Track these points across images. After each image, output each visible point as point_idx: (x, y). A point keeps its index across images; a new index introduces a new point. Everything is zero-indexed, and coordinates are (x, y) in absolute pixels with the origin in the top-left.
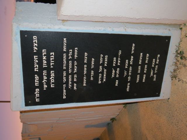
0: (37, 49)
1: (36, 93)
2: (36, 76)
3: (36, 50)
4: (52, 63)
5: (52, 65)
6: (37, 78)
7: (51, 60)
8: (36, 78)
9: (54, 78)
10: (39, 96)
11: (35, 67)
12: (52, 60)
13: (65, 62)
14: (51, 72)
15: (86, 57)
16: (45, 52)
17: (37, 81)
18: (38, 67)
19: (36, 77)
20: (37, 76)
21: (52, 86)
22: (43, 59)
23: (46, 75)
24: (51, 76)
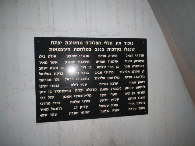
2: (60, 42)
3: (136, 56)
4: (42, 98)
5: (111, 95)
6: (58, 43)
8: (59, 42)
9: (94, 44)
10: (40, 88)
11: (69, 42)
14: (100, 42)
15: (113, 50)
17: (56, 43)
18: (69, 44)
19: (59, 42)
21: (87, 43)
23: (68, 51)
24: (97, 42)
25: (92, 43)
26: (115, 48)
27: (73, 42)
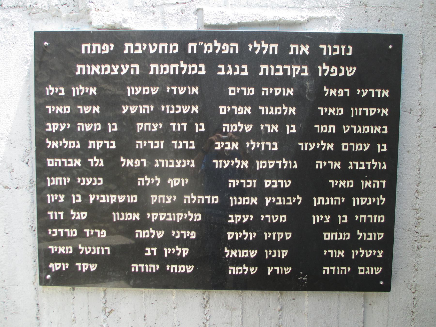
0: (363, 96)
1: (216, 44)
2: (110, 47)
3: (361, 93)
7: (381, 182)
8: (105, 45)
12: (382, 183)
13: (371, 239)
16: (150, 271)
17: (97, 48)
19: (107, 46)
20: (109, 50)
22: (193, 107)
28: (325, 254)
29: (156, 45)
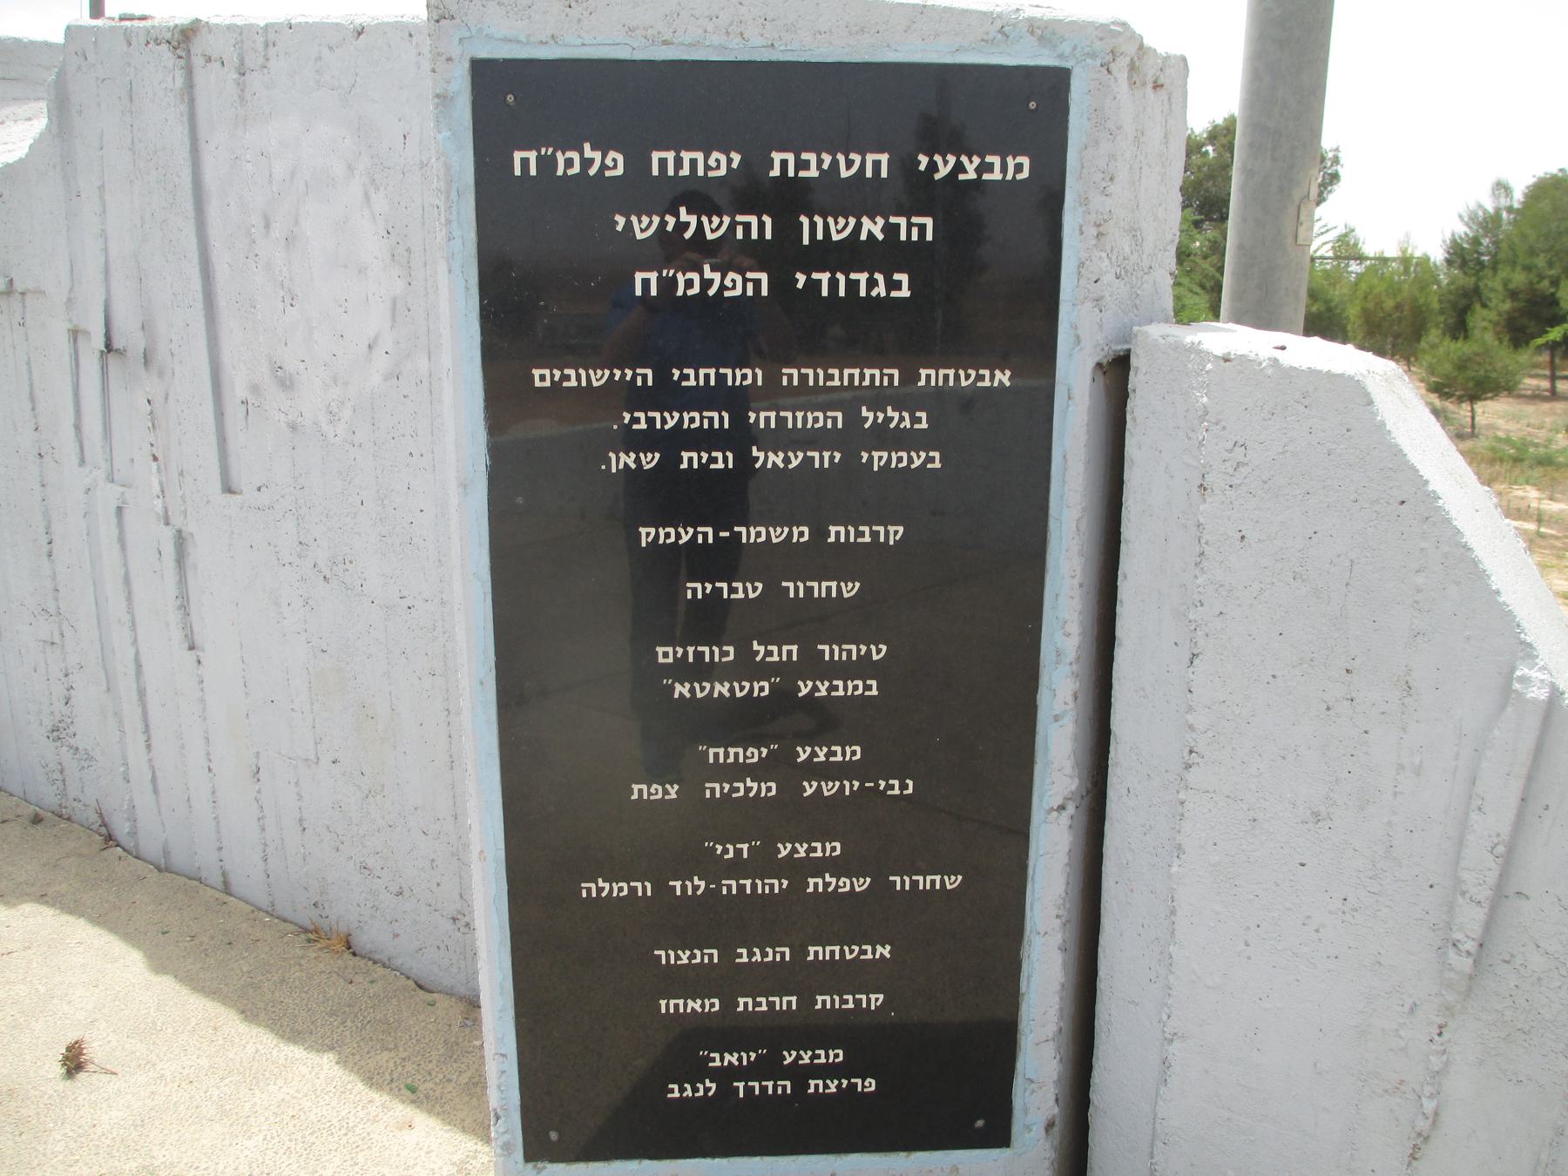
2: (730, 161)
3: (933, 167)
6: (712, 163)
8: (715, 155)
11: (804, 156)
15: (867, 539)
17: (693, 162)
18: (802, 174)
25: (569, 163)
26: (650, 414)
27: (841, 158)
28: (800, 285)
29: (856, 158)
